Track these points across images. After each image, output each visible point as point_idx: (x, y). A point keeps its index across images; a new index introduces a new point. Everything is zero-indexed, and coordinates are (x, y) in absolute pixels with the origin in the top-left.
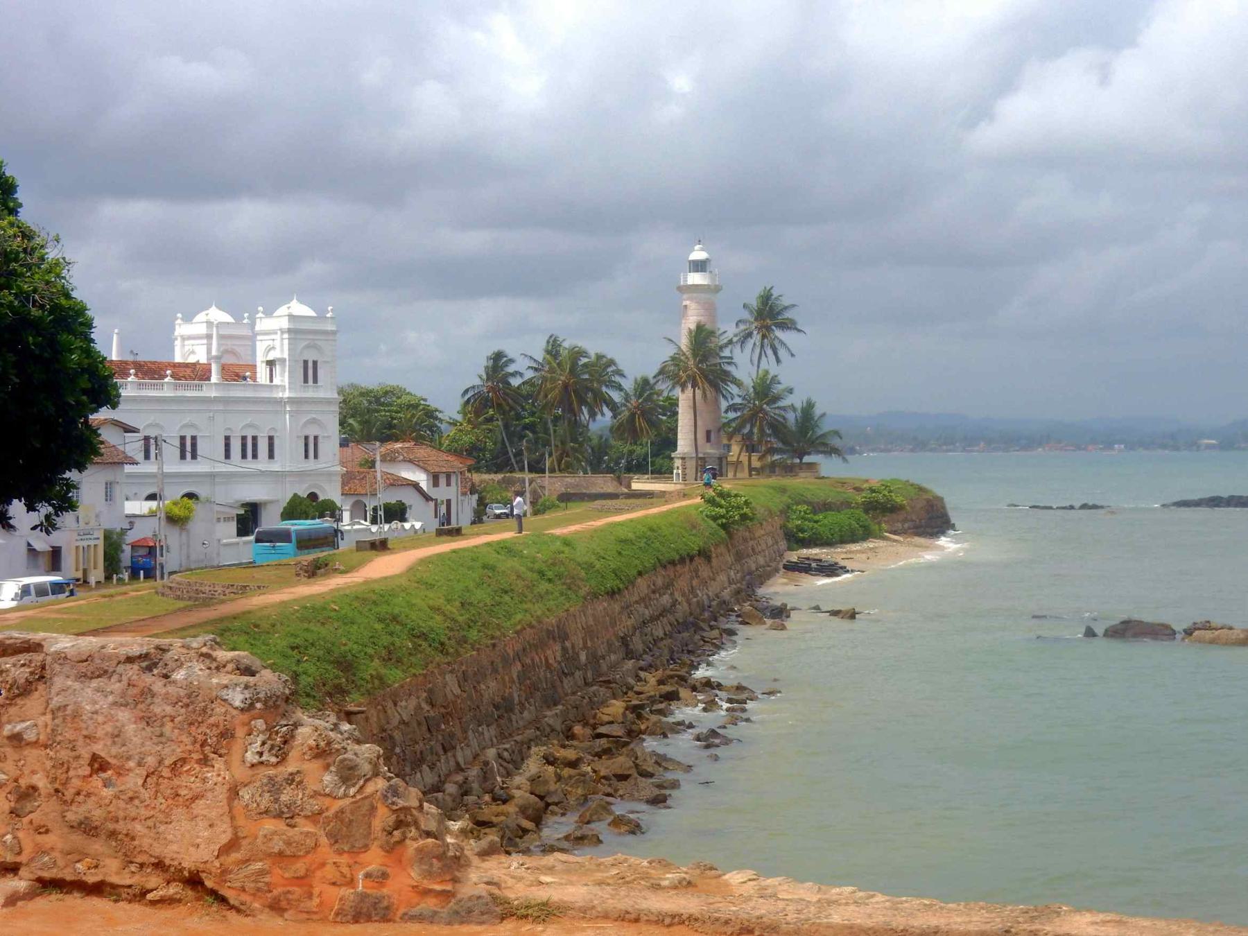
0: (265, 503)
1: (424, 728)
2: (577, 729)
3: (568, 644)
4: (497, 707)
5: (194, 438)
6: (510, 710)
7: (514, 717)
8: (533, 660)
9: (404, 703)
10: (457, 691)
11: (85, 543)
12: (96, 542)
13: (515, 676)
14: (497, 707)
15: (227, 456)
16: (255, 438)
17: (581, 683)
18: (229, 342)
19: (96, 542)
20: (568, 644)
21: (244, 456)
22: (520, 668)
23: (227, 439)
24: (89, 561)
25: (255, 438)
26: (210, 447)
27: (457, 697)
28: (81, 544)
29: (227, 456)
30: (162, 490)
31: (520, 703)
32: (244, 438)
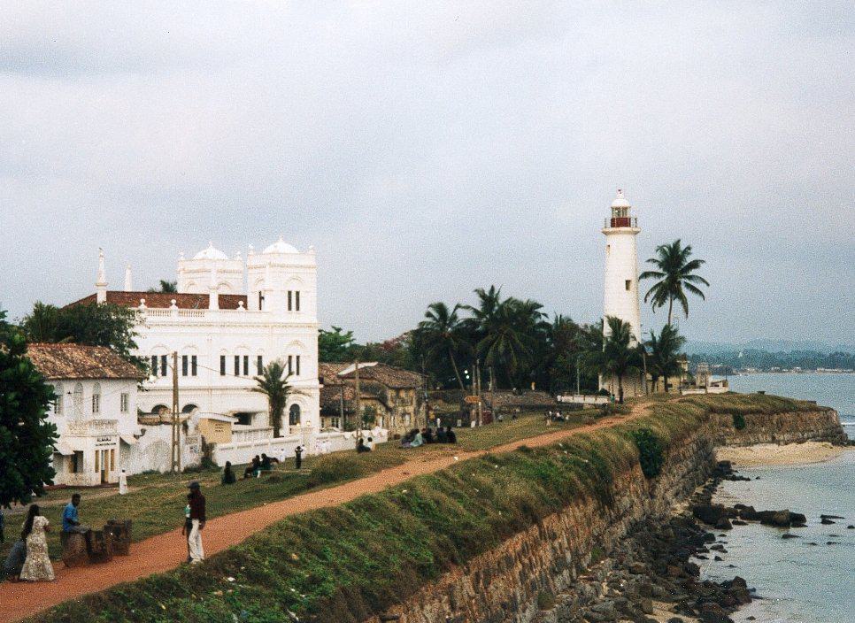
0: (254, 414)
2: (16, 453)
3: (556, 544)
5: (194, 358)
6: (515, 609)
7: (518, 616)
8: (530, 560)
10: (472, 593)
11: (104, 448)
12: (112, 447)
13: (517, 576)
14: (504, 606)
15: (223, 373)
16: (246, 358)
18: (225, 275)
19: (112, 447)
20: (556, 544)
21: (237, 373)
22: (520, 566)
23: (223, 358)
24: (106, 466)
25: (246, 358)
26: (208, 365)
27: (471, 598)
28: (100, 448)
29: (223, 373)
30: (251, 313)
31: (522, 602)
32: (237, 358)
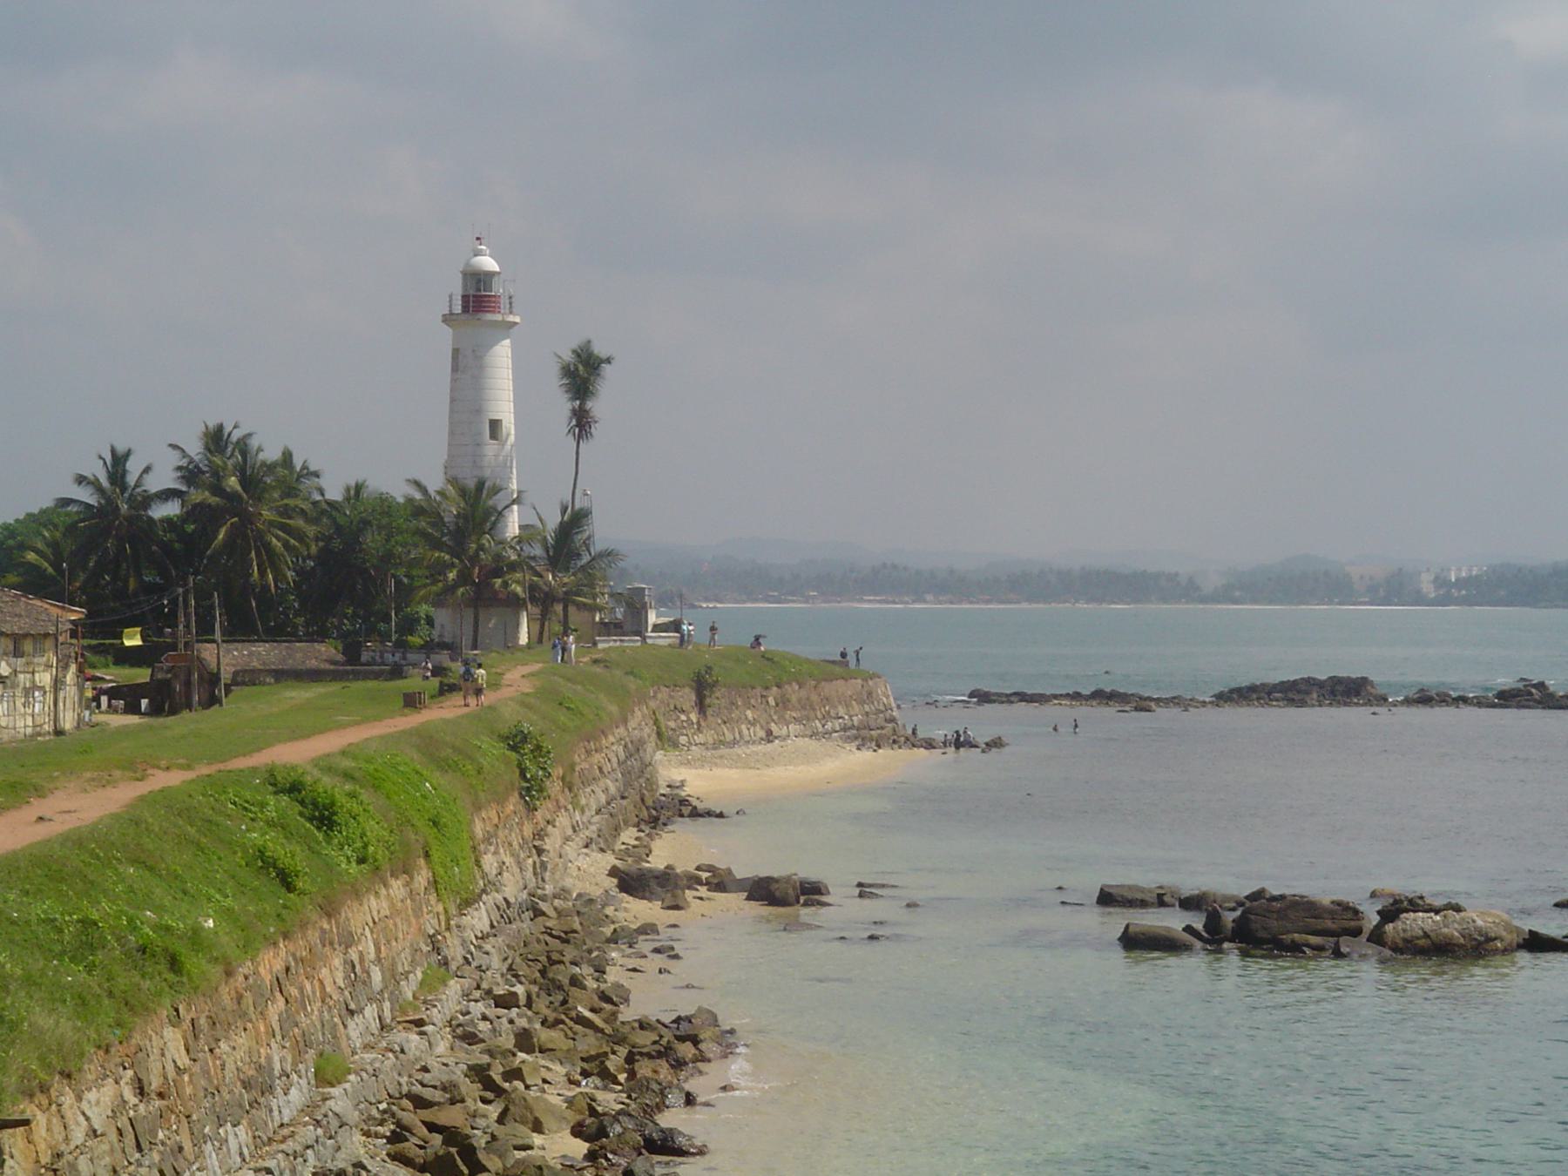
1: (130, 1139)
4: (247, 1085)
9: (91, 1096)
10: (184, 1060)
17: (375, 1026)
